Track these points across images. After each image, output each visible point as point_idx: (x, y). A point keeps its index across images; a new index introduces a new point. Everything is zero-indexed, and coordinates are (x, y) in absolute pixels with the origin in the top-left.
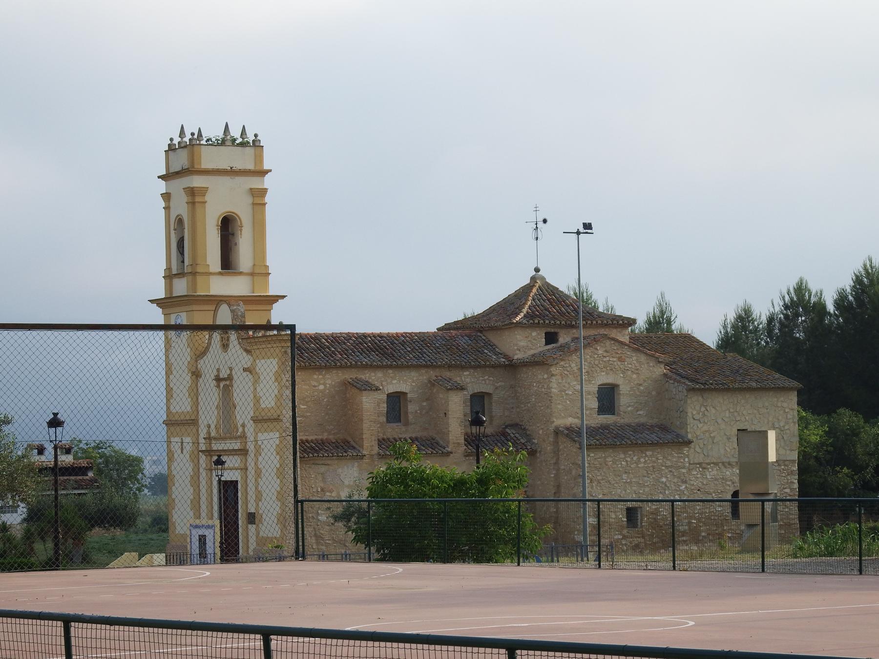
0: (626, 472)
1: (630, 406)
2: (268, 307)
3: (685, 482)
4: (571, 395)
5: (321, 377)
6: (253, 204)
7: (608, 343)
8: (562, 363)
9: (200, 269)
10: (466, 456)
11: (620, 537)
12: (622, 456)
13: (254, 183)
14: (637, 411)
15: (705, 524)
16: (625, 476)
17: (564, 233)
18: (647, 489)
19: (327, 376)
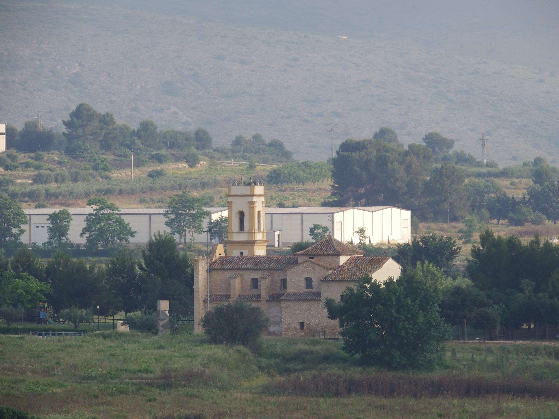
0: (298, 310)
1: (316, 286)
2: (253, 245)
3: (320, 314)
4: (294, 281)
5: (227, 272)
6: (250, 207)
7: (308, 263)
8: (291, 270)
9: (229, 231)
10: (267, 302)
11: (296, 332)
12: (297, 304)
13: (249, 199)
14: (319, 287)
15: (328, 329)
16: (298, 311)
17: (392, 234)
18: (306, 316)
19: (230, 272)
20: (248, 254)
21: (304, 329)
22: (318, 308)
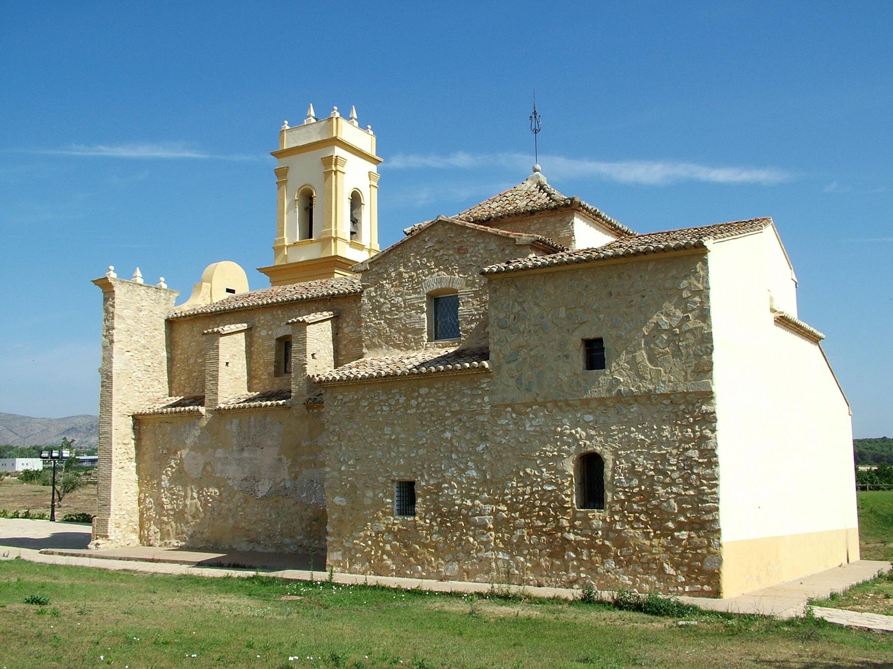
5: (475, 215)
20: (250, 290)
21: (414, 514)
22: (474, 413)
